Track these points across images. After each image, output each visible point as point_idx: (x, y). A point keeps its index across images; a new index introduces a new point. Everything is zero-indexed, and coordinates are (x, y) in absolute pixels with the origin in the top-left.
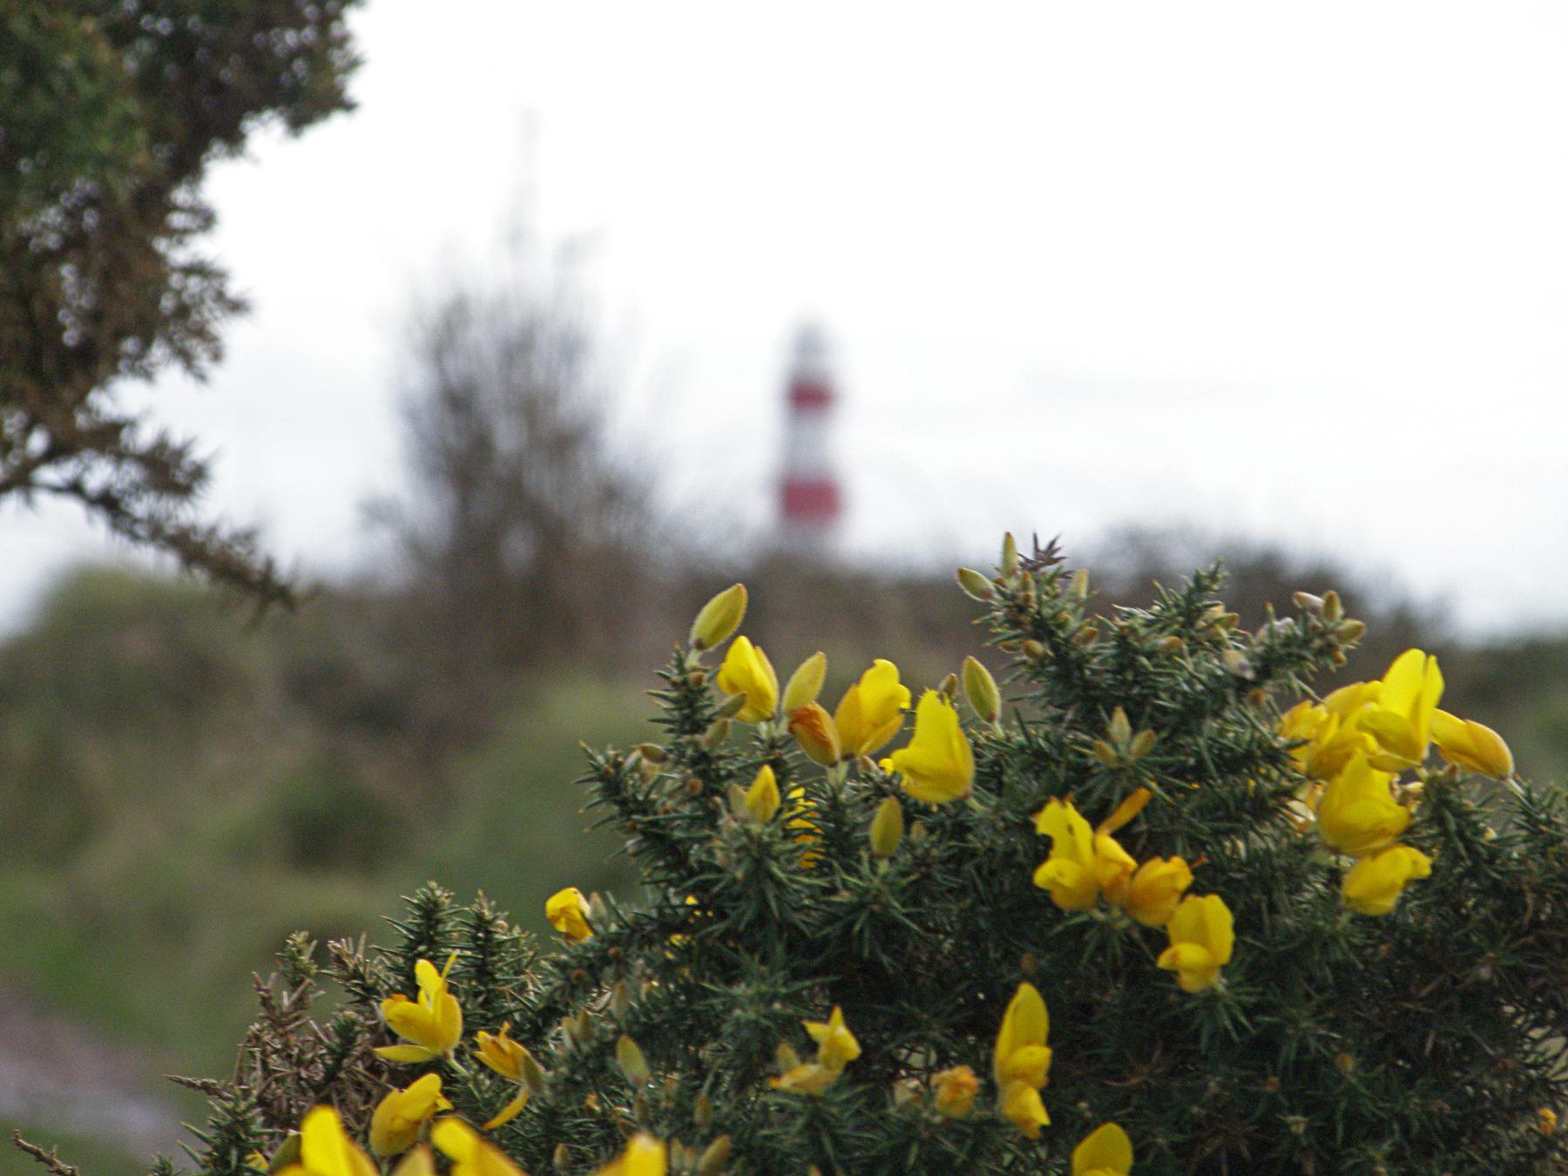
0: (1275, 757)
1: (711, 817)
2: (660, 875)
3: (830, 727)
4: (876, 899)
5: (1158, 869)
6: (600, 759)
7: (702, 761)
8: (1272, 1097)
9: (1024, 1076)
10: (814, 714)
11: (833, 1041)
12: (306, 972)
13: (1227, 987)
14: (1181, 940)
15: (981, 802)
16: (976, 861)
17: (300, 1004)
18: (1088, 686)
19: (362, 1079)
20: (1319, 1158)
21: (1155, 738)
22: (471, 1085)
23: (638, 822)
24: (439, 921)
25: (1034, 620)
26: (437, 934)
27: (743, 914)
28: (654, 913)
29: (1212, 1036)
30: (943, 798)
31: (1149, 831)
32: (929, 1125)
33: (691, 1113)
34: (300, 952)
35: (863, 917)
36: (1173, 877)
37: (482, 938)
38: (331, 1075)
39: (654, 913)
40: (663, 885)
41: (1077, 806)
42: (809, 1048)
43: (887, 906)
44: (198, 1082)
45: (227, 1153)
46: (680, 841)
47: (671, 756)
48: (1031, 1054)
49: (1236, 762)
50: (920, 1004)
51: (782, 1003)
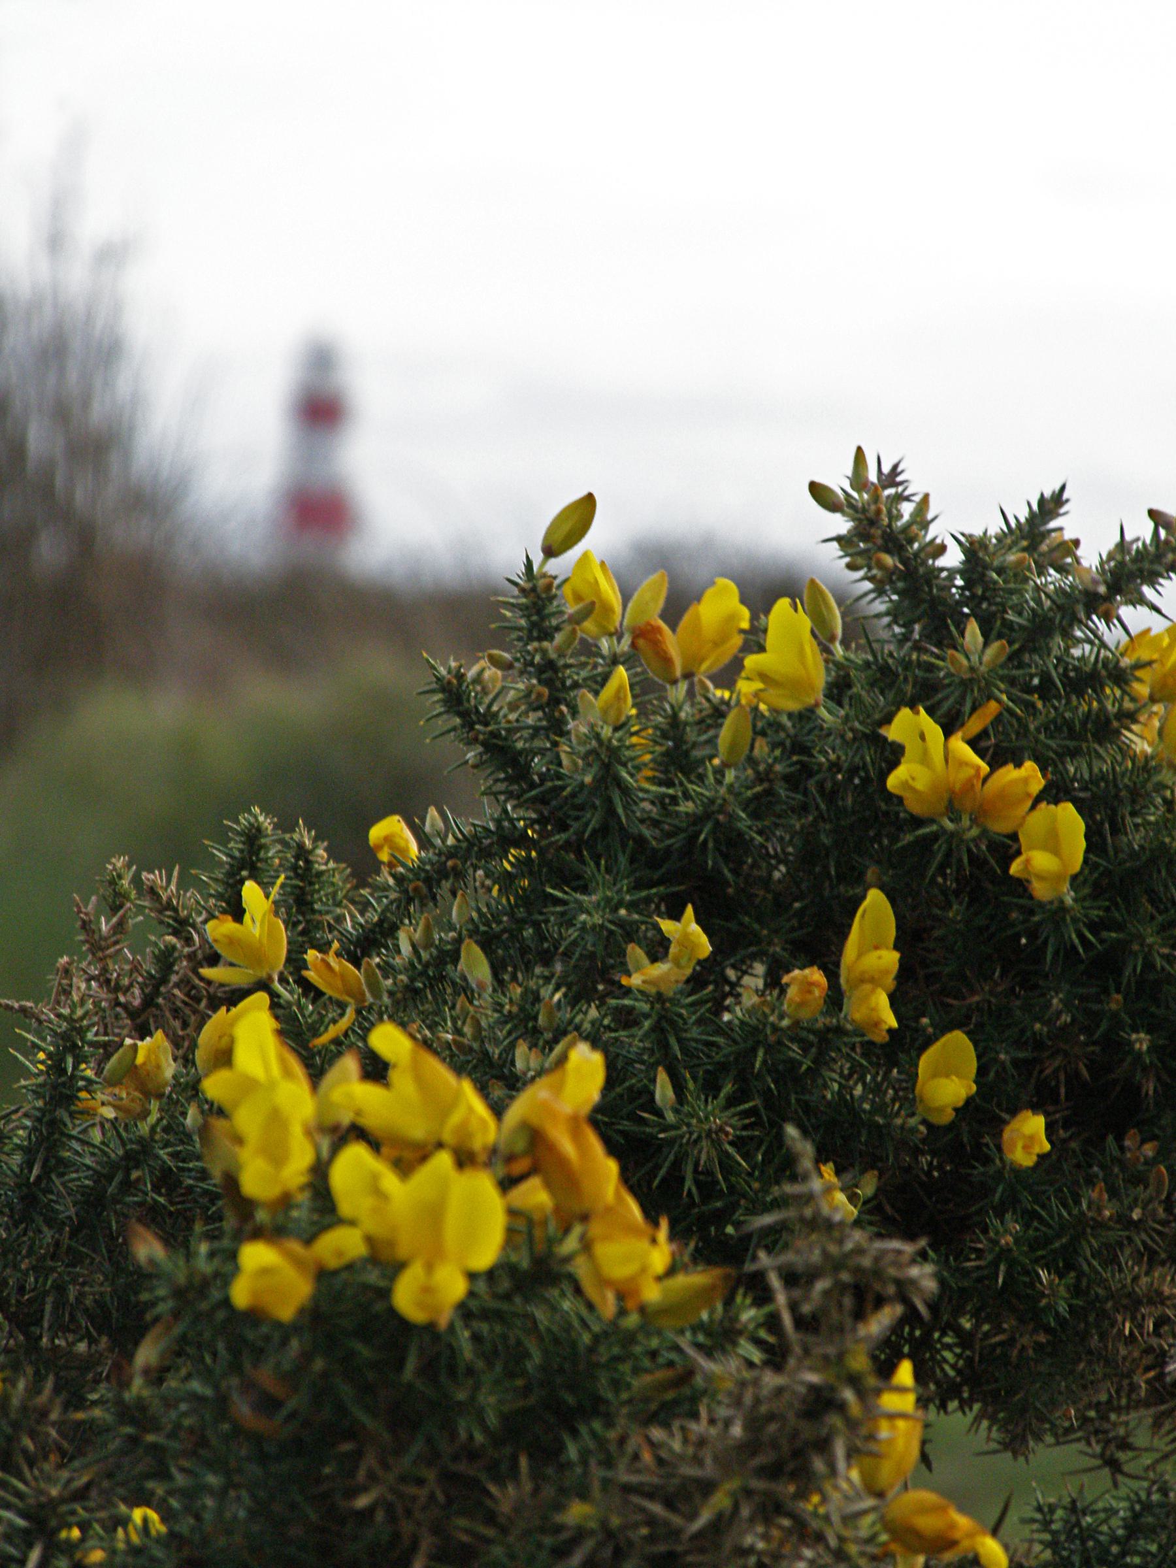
0: (1120, 677)
1: (557, 727)
2: (501, 786)
3: (672, 643)
4: (721, 810)
5: (1009, 774)
6: (443, 671)
7: (548, 671)
8: (1115, 1015)
9: (873, 980)
10: (658, 630)
11: (686, 939)
12: (126, 896)
13: (1075, 900)
14: (1031, 848)
15: (830, 712)
16: (818, 777)
17: (119, 928)
18: (934, 602)
19: (179, 1004)
20: (1159, 1079)
21: (1008, 650)
22: (295, 1008)
23: (479, 732)
24: (261, 847)
25: (884, 532)
26: (259, 860)
27: (587, 825)
28: (492, 826)
29: (1056, 953)
30: (793, 706)
31: (996, 745)
32: (775, 1029)
33: (535, 1018)
34: (120, 877)
35: (708, 827)
36: (1026, 781)
37: (303, 873)
38: (149, 1001)
39: (492, 826)
40: (502, 798)
41: (930, 712)
42: (658, 948)
43: (732, 817)
44: (16, 1005)
45: (63, 1060)
46: (520, 753)
47: (517, 665)
48: (880, 958)
49: (1087, 679)
50: (758, 920)
51: (627, 909)
